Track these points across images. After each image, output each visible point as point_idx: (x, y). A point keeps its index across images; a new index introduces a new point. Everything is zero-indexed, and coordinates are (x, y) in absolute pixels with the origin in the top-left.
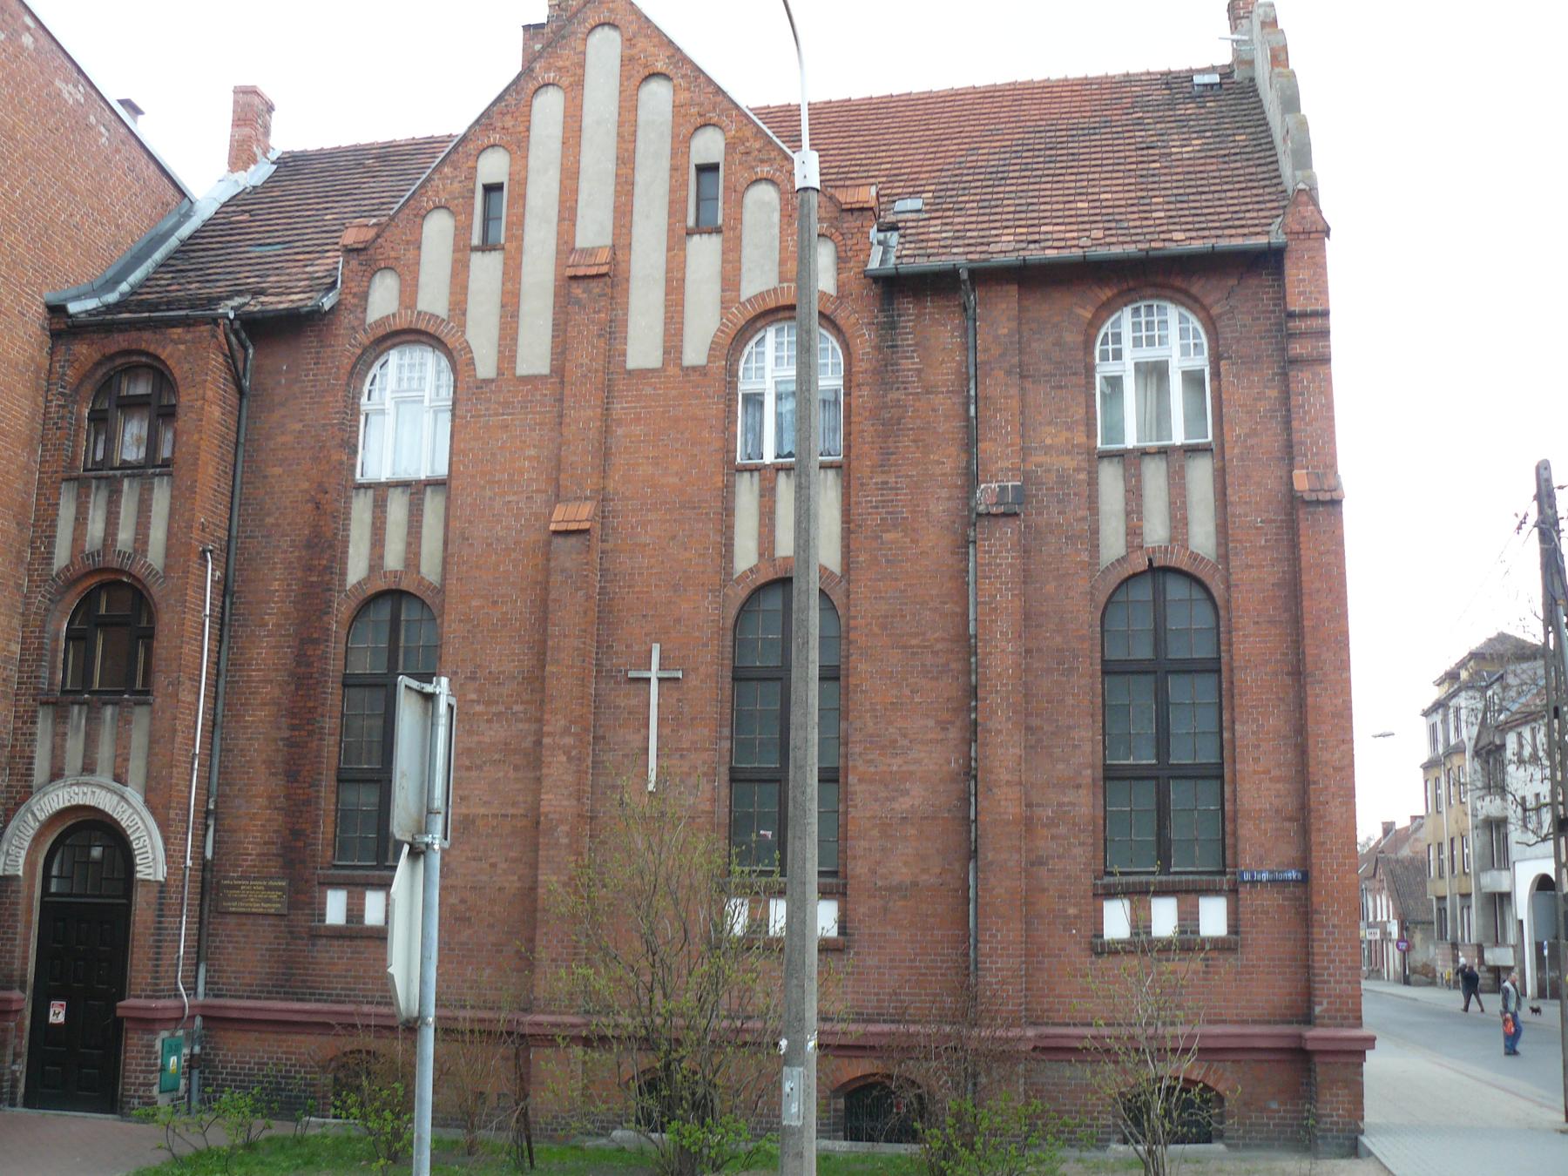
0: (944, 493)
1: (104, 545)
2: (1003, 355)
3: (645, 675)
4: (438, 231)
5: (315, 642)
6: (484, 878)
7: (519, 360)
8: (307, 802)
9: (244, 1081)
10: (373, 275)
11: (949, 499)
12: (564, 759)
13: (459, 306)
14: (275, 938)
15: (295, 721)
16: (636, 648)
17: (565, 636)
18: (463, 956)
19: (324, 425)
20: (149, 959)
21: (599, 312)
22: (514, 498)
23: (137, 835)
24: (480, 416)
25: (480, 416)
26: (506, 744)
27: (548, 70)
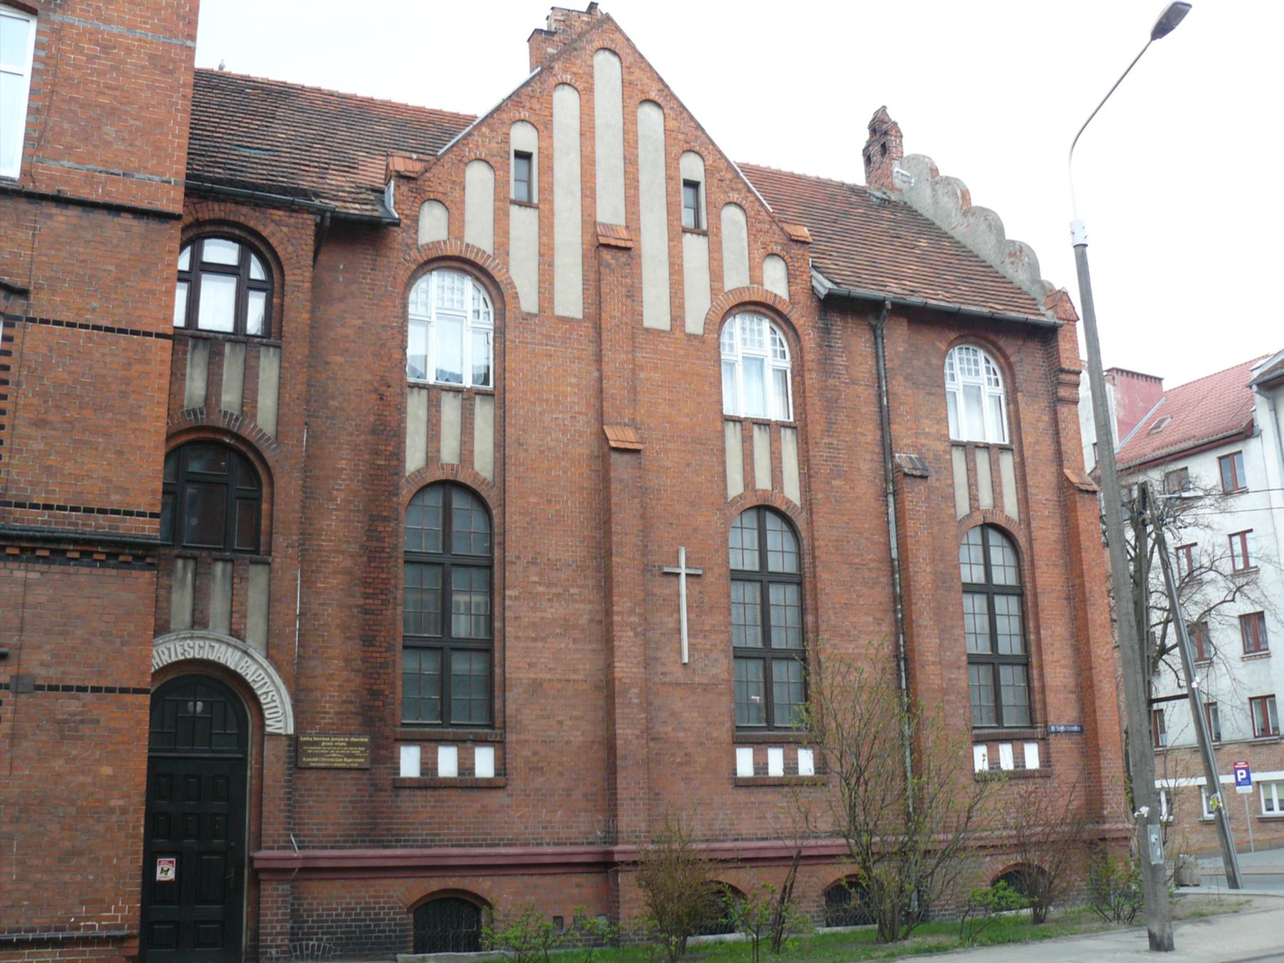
0: (868, 456)
1: (206, 404)
2: (901, 366)
3: (677, 571)
4: (478, 179)
5: (385, 519)
6: (553, 733)
7: (556, 303)
8: (384, 665)
9: (332, 927)
10: (423, 203)
11: (871, 461)
12: (631, 634)
14: (359, 790)
15: (368, 591)
16: (666, 549)
17: (626, 534)
18: (538, 800)
19: (384, 326)
20: (281, 811)
21: (626, 277)
22: (561, 416)
23: (264, 690)
24: (527, 343)
25: (527, 343)
26: (565, 620)
27: (566, 71)
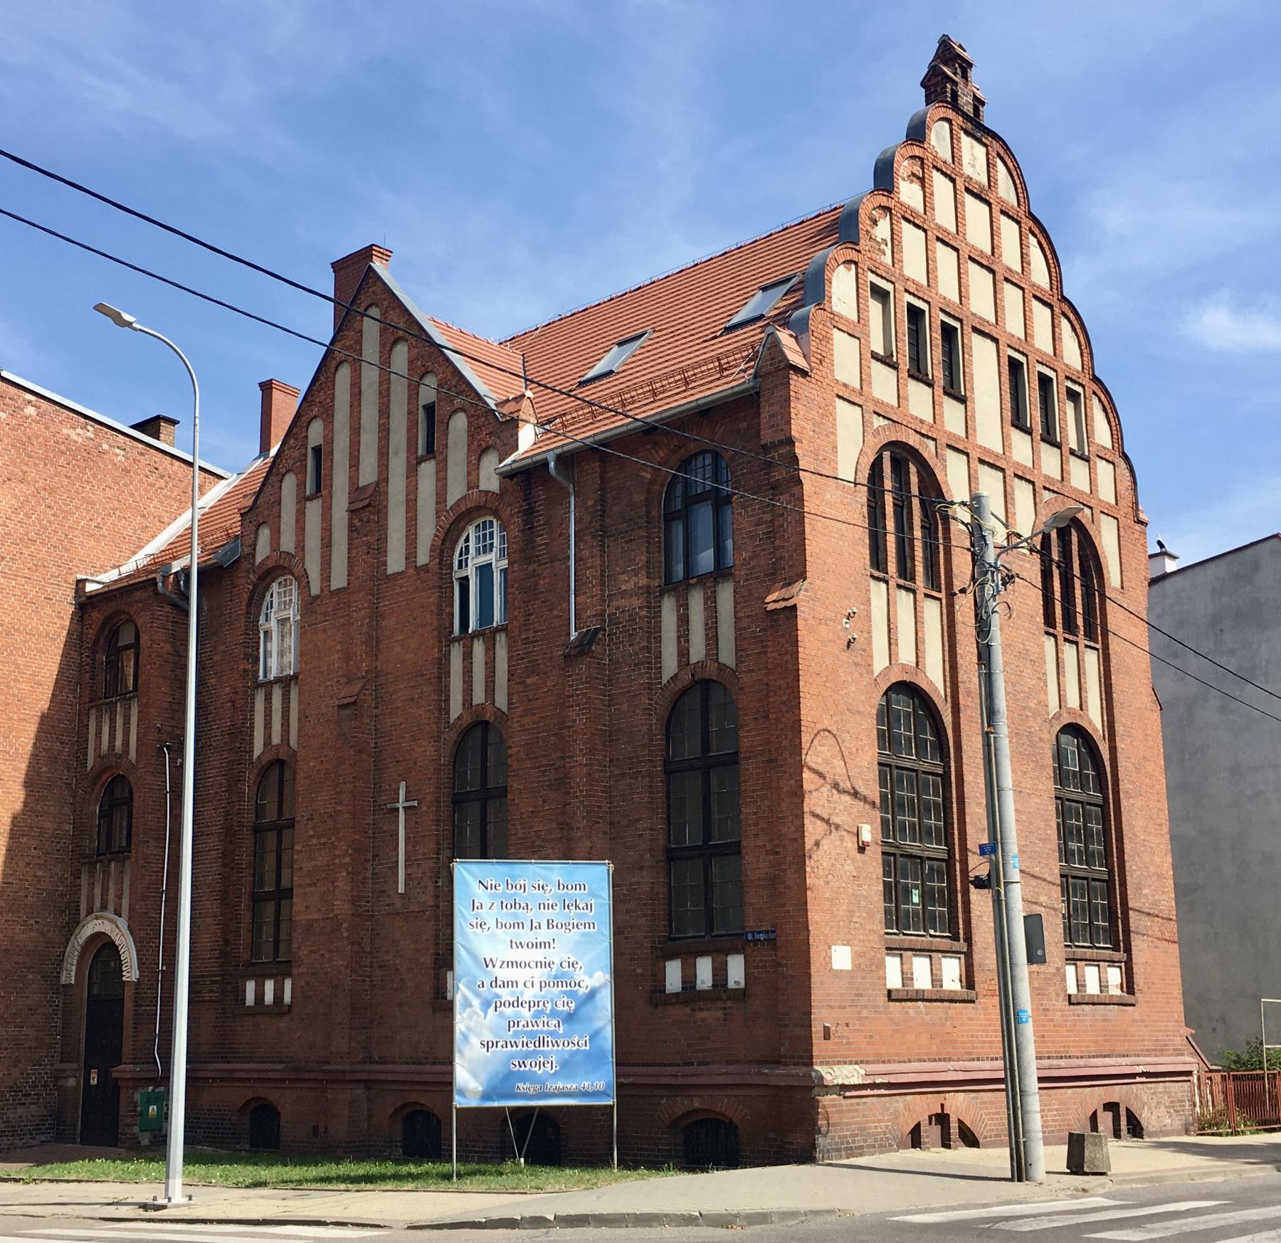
13: (300, 545)
